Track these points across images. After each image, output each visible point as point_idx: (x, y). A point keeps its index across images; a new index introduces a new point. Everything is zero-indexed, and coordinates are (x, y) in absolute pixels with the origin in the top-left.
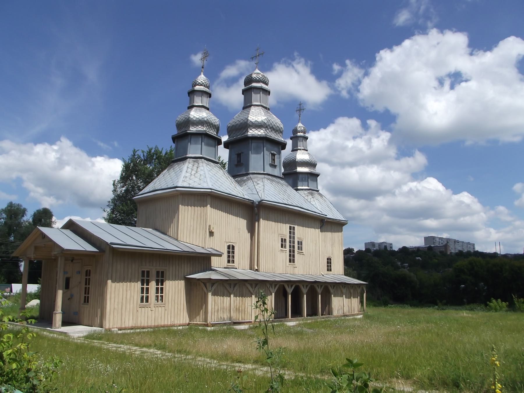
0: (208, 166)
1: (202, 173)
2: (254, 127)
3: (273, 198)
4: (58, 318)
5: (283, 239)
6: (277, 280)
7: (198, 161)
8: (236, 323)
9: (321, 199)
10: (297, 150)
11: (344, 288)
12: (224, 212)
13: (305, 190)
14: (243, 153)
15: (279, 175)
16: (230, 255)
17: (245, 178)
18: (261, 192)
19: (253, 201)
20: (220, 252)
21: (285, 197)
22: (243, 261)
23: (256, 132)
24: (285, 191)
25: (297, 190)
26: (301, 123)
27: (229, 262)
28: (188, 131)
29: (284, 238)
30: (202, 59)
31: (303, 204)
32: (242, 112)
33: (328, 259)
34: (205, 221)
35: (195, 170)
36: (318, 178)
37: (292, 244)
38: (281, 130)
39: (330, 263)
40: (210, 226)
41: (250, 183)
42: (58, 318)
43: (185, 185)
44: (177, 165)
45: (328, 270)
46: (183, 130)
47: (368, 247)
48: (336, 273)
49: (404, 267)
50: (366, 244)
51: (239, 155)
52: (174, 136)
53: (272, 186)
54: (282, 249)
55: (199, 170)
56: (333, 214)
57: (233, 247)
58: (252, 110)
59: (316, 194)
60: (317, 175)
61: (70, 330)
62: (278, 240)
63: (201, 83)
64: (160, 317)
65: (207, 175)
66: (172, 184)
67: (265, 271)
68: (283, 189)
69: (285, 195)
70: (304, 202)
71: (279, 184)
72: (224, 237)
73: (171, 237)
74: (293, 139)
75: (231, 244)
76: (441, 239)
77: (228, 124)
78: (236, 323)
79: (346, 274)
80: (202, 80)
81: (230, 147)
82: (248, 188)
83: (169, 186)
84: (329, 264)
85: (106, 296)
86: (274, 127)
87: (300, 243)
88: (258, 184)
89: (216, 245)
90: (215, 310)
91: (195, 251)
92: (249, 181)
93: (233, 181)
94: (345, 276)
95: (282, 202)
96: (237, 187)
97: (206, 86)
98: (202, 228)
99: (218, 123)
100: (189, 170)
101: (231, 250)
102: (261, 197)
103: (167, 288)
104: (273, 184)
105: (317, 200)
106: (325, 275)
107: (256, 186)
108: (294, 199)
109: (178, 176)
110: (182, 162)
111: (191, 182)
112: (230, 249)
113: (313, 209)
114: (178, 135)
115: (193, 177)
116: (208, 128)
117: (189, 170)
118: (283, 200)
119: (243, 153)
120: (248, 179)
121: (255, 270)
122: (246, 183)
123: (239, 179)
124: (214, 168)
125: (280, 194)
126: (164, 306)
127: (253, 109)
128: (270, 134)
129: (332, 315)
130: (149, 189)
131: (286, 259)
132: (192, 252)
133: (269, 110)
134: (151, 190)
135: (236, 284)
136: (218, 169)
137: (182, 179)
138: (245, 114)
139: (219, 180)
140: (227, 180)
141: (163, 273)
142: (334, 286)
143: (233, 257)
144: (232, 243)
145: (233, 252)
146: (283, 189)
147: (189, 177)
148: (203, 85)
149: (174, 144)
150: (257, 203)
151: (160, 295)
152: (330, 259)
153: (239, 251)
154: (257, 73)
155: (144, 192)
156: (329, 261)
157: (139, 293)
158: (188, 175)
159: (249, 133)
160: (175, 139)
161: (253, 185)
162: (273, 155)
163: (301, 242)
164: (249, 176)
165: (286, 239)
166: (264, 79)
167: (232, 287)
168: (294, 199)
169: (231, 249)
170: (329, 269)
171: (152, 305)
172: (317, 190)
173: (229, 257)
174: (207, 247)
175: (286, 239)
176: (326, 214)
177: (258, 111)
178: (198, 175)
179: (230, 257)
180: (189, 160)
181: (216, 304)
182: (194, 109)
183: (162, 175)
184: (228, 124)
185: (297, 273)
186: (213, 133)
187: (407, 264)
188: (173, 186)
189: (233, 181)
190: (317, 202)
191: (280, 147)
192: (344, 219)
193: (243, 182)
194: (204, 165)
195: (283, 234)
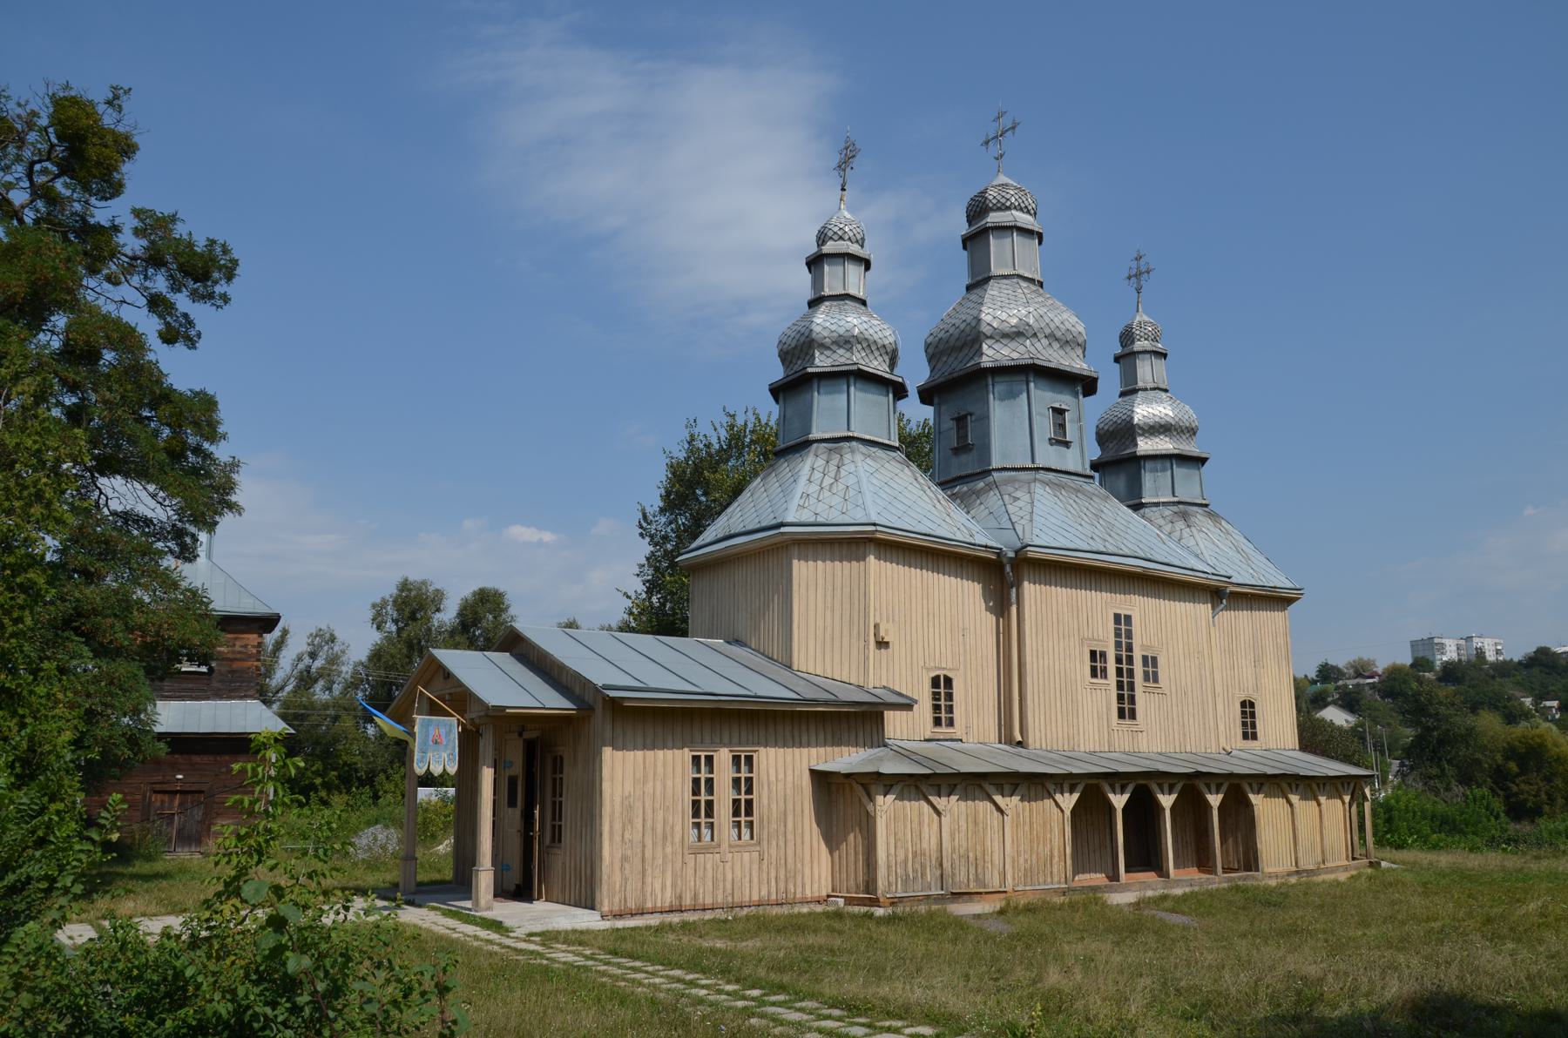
1: (851, 480)
2: (997, 338)
4: (485, 879)
6: (1075, 771)
7: (842, 448)
8: (957, 896)
9: (1212, 529)
10: (1135, 391)
11: (1294, 789)
12: (962, 579)
13: (1164, 504)
14: (971, 415)
15: (1079, 470)
16: (940, 706)
17: (981, 484)
18: (1023, 522)
19: (1001, 549)
20: (907, 697)
21: (1096, 531)
22: (981, 721)
23: (1005, 351)
24: (1096, 515)
25: (1137, 507)
26: (1144, 312)
27: (937, 722)
28: (810, 370)
29: (1098, 650)
30: (840, 167)
31: (1155, 548)
32: (963, 298)
33: (1243, 704)
34: (862, 614)
35: (832, 474)
37: (1125, 666)
38: (1080, 340)
39: (1253, 715)
40: (876, 626)
41: (993, 499)
42: (485, 879)
43: (806, 516)
44: (786, 464)
45: (1245, 736)
46: (796, 368)
47: (1420, 655)
48: (1272, 745)
49: (1544, 713)
50: (1414, 644)
51: (961, 421)
52: (775, 385)
53: (1058, 502)
54: (1094, 680)
55: (843, 473)
56: (1251, 571)
57: (949, 682)
58: (992, 293)
59: (1198, 516)
61: (512, 913)
62: (1081, 653)
63: (840, 233)
64: (747, 879)
65: (865, 487)
66: (772, 516)
67: (1044, 747)
68: (1090, 508)
69: (1098, 525)
71: (1079, 495)
72: (921, 655)
73: (772, 659)
74: (1121, 361)
75: (941, 673)
78: (957, 896)
79: (1304, 747)
80: (841, 226)
81: (936, 400)
82: (987, 511)
83: (764, 524)
84: (1249, 720)
85: (601, 825)
86: (1059, 334)
87: (1150, 661)
88: (1016, 499)
89: (897, 678)
90: (898, 859)
91: (833, 697)
92: (992, 493)
93: (940, 497)
94: (1300, 753)
95: (1088, 548)
96: (952, 514)
97: (854, 239)
98: (855, 631)
99: (891, 340)
100: (817, 475)
101: (942, 690)
102: (1021, 537)
104: (1061, 497)
106: (1234, 753)
107: (1009, 507)
108: (1127, 536)
109: (786, 493)
110: (798, 455)
111: (820, 508)
112: (939, 688)
114: (786, 380)
115: (827, 493)
116: (864, 354)
117: (817, 475)
118: (1091, 541)
119: (971, 415)
120: (989, 487)
121: (1014, 743)
122: (983, 498)
123: (965, 488)
124: (887, 465)
125: (1083, 523)
126: (758, 848)
127: (993, 290)
128: (1047, 355)
129: (1257, 870)
130: (714, 534)
131: (1109, 709)
132: (826, 703)
133: (1042, 287)
134: (720, 535)
135: (955, 785)
136: (898, 465)
137: (796, 500)
138: (972, 305)
139: (900, 497)
140: (925, 497)
142: (1324, 784)
143: (950, 709)
144: (944, 669)
145: (950, 697)
146: (1090, 508)
147: (815, 495)
148: (847, 237)
149: (777, 406)
150: (1011, 554)
151: (706, 823)
152: (1252, 705)
153: (966, 690)
154: (999, 185)
155: (703, 543)
156: (1248, 709)
157: (686, 817)
158: (814, 488)
159: (984, 358)
160: (778, 391)
161: (1001, 502)
162: (1059, 412)
163: (1154, 659)
164: (990, 479)
165: (1105, 652)
167: (1294, 789)
168: (1127, 536)
169: (942, 686)
170: (1250, 733)
171: (725, 845)
172: (1204, 502)
173: (937, 708)
174: (871, 686)
175: (1105, 652)
176: (1230, 573)
177: (1010, 292)
178: (841, 487)
179: (940, 709)
180: (817, 448)
181: (899, 844)
182: (823, 308)
183: (749, 495)
185: (1144, 747)
186: (878, 366)
187: (1555, 704)
188: (774, 522)
189: (940, 497)
191: (1080, 389)
192: (1289, 585)
193: (974, 497)
194: (859, 458)
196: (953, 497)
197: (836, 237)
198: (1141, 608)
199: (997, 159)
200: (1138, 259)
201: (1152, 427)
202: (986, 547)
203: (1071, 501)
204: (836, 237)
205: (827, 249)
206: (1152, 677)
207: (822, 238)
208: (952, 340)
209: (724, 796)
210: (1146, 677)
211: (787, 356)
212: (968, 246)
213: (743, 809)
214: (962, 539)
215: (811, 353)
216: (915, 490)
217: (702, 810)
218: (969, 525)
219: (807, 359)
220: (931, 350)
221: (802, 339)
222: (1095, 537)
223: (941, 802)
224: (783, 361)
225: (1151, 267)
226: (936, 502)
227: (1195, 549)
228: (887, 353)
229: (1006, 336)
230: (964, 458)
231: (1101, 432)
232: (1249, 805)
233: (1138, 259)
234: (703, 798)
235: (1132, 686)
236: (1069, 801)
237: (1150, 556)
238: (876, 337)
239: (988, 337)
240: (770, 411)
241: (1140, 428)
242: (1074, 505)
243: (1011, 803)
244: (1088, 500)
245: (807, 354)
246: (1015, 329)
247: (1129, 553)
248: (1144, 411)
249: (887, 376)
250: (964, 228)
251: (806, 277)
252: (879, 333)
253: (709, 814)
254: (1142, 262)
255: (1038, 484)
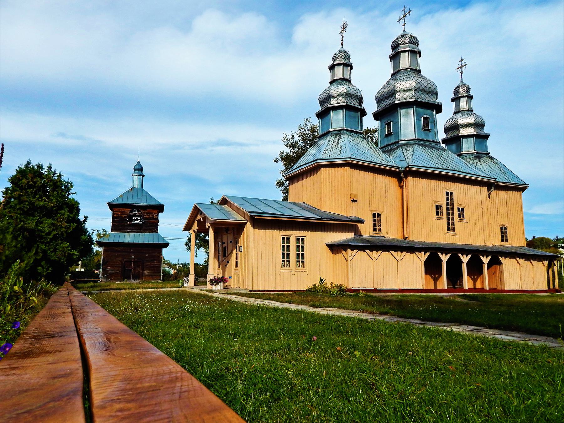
0: (350, 137)
3: (423, 163)
5: (438, 206)
10: (459, 112)
18: (409, 158)
21: (439, 161)
24: (440, 156)
25: (460, 155)
27: (375, 230)
30: (341, 32)
36: (489, 141)
52: (318, 113)
55: (340, 141)
57: (379, 215)
60: (486, 137)
68: (438, 153)
69: (440, 159)
70: (465, 166)
76: (523, 301)
77: (467, 126)
86: (426, 89)
87: (461, 211)
88: (407, 150)
92: (399, 149)
100: (331, 143)
103: (278, 259)
104: (425, 149)
105: (485, 164)
108: (452, 163)
109: (320, 150)
113: (477, 173)
117: (331, 143)
118: (436, 165)
124: (357, 139)
136: (362, 139)
139: (361, 149)
141: (303, 239)
143: (380, 225)
147: (330, 149)
160: (320, 115)
161: (402, 152)
166: (412, 40)
172: (487, 153)
176: (496, 177)
184: (467, 126)
189: (377, 150)
190: (485, 165)
195: (438, 200)
196: (385, 152)
197: (339, 58)
198: (457, 189)
199: (403, 26)
200: (462, 61)
201: (466, 125)
202: (394, 166)
203: (430, 151)
204: (339, 58)
205: (335, 63)
206: (461, 215)
207: (334, 59)
208: (385, 94)
209: (293, 252)
210: (459, 216)
211: (322, 103)
212: (392, 60)
213: (300, 256)
214: (384, 163)
215: (330, 100)
216: (367, 147)
217: (285, 256)
218: (387, 159)
219: (329, 102)
220: (377, 100)
221: (327, 95)
222: (438, 163)
223: (533, 262)
224: (321, 105)
225: (467, 63)
226: (375, 151)
227: (482, 169)
228: (358, 99)
229: (404, 91)
230: (389, 138)
231: (446, 128)
232: (500, 263)
233: (462, 61)
234: (286, 260)
235: (453, 219)
236: (424, 256)
237: (461, 170)
238: (353, 93)
239: (398, 92)
240: (316, 122)
241: (461, 125)
242: (431, 152)
243: (522, 261)
244: (437, 151)
245: (328, 101)
246: (408, 88)
247: (452, 169)
248: (462, 120)
249: (358, 107)
250: (391, 53)
251: (329, 73)
252: (355, 91)
253: (288, 258)
254: (463, 62)
255: (416, 145)
